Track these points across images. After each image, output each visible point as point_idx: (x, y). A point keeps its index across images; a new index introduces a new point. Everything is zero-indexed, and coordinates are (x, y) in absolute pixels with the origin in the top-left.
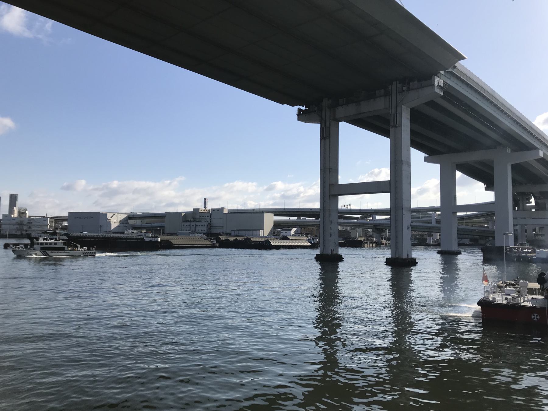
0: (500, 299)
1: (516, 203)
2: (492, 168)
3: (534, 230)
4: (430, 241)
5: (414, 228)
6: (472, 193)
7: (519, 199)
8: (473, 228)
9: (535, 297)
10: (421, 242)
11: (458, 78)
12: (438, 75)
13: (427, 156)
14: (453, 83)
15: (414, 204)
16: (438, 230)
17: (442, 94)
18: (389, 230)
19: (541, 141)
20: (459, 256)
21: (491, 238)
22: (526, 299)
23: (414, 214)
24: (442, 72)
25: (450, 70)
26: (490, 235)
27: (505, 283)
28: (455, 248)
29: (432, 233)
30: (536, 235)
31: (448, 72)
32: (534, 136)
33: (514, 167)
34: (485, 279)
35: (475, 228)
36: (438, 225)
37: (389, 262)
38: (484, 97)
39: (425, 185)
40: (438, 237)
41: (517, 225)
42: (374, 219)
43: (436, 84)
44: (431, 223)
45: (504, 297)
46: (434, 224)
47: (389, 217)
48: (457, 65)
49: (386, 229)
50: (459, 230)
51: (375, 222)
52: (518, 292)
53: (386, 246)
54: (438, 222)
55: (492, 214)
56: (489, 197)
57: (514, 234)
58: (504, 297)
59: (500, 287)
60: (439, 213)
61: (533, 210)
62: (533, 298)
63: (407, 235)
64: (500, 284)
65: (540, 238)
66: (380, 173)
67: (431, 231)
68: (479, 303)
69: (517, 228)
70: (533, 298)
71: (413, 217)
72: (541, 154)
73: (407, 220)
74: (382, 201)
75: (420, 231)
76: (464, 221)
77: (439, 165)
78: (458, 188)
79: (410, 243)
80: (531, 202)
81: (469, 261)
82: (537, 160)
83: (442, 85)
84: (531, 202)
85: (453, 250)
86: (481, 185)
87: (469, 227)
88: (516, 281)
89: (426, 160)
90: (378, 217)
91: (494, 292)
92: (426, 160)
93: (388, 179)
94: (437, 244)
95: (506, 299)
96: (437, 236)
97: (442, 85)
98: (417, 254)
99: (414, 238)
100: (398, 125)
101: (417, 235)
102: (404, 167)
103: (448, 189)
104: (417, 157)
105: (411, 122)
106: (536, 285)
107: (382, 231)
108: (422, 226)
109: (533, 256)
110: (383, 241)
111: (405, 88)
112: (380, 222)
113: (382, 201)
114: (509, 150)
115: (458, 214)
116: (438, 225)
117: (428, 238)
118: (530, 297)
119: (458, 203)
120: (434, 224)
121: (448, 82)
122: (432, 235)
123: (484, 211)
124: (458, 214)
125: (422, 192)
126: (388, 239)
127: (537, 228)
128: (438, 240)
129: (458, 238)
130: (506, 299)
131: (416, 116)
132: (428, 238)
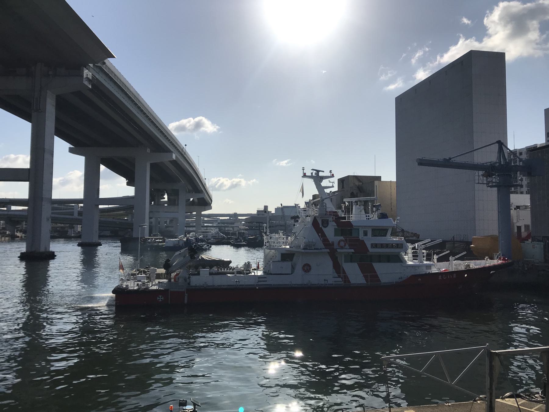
0: (132, 285)
1: (152, 198)
2: (134, 165)
3: (166, 222)
4: (71, 233)
5: (54, 220)
6: (114, 186)
7: (156, 195)
8: (114, 220)
9: (161, 281)
10: (62, 234)
11: (107, 75)
12: (88, 67)
13: (72, 146)
14: (100, 77)
15: (56, 195)
16: (79, 222)
17: (90, 87)
18: (26, 222)
19: (175, 146)
20: (99, 248)
21: (130, 230)
22: (154, 283)
23: (56, 205)
24: (91, 65)
25: (99, 65)
26: (129, 226)
27: (138, 270)
28: (95, 239)
29: (74, 225)
30: (166, 227)
31: (97, 66)
32: (169, 140)
33: (152, 165)
34: (121, 267)
35: (116, 220)
36: (80, 217)
37: (23, 257)
38: (129, 98)
39: (68, 177)
40: (79, 229)
41: (152, 218)
42: (9, 210)
43: (85, 76)
44: (73, 215)
45: (136, 283)
46: (76, 215)
47: (26, 208)
48: (106, 61)
49: (23, 221)
50: (100, 222)
51: (10, 213)
52: (148, 278)
53: (22, 240)
54: (80, 213)
55: (132, 207)
56: (130, 191)
57: (150, 226)
58: (136, 283)
59: (133, 275)
60: (82, 205)
61: (166, 205)
62: (159, 282)
63: (46, 227)
64: (134, 272)
65: (170, 229)
66: (16, 159)
67: (73, 223)
68: (114, 292)
69: (152, 220)
70: (159, 282)
71: (53, 209)
72: (174, 157)
73: (46, 211)
74: (20, 190)
75: (60, 223)
76: (106, 214)
77: (84, 157)
78: (101, 181)
79: (49, 235)
80: (164, 198)
81: (109, 253)
82: (170, 161)
83: (91, 78)
84: (164, 198)
85: (94, 241)
86: (123, 181)
87: (110, 219)
88: (147, 268)
89: (71, 151)
90: (13, 208)
91: (128, 280)
92: (71, 151)
93: (28, 166)
94: (78, 236)
95: (138, 285)
96: (79, 228)
97: (91, 78)
98: (55, 247)
99: (54, 230)
100: (41, 111)
101: (57, 227)
102: (47, 156)
103: (92, 181)
104: (61, 147)
105: (56, 109)
106: (162, 271)
107: (19, 223)
108: (64, 218)
109: (163, 245)
110: (18, 234)
111: (50, 73)
112: (21, 213)
113: (20, 190)
114: (148, 150)
115: (100, 207)
116: (80, 217)
117: (69, 230)
118: (157, 281)
119: (102, 196)
120: (76, 215)
121: (97, 77)
122: (74, 228)
123: (123, 203)
124: (100, 207)
125: (64, 183)
126: (24, 232)
127: (168, 221)
128: (79, 232)
129: (99, 230)
130: (138, 285)
131: (62, 104)
132: (69, 230)
